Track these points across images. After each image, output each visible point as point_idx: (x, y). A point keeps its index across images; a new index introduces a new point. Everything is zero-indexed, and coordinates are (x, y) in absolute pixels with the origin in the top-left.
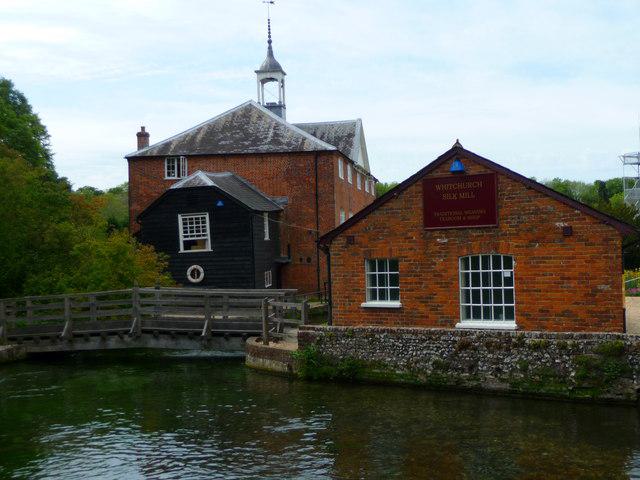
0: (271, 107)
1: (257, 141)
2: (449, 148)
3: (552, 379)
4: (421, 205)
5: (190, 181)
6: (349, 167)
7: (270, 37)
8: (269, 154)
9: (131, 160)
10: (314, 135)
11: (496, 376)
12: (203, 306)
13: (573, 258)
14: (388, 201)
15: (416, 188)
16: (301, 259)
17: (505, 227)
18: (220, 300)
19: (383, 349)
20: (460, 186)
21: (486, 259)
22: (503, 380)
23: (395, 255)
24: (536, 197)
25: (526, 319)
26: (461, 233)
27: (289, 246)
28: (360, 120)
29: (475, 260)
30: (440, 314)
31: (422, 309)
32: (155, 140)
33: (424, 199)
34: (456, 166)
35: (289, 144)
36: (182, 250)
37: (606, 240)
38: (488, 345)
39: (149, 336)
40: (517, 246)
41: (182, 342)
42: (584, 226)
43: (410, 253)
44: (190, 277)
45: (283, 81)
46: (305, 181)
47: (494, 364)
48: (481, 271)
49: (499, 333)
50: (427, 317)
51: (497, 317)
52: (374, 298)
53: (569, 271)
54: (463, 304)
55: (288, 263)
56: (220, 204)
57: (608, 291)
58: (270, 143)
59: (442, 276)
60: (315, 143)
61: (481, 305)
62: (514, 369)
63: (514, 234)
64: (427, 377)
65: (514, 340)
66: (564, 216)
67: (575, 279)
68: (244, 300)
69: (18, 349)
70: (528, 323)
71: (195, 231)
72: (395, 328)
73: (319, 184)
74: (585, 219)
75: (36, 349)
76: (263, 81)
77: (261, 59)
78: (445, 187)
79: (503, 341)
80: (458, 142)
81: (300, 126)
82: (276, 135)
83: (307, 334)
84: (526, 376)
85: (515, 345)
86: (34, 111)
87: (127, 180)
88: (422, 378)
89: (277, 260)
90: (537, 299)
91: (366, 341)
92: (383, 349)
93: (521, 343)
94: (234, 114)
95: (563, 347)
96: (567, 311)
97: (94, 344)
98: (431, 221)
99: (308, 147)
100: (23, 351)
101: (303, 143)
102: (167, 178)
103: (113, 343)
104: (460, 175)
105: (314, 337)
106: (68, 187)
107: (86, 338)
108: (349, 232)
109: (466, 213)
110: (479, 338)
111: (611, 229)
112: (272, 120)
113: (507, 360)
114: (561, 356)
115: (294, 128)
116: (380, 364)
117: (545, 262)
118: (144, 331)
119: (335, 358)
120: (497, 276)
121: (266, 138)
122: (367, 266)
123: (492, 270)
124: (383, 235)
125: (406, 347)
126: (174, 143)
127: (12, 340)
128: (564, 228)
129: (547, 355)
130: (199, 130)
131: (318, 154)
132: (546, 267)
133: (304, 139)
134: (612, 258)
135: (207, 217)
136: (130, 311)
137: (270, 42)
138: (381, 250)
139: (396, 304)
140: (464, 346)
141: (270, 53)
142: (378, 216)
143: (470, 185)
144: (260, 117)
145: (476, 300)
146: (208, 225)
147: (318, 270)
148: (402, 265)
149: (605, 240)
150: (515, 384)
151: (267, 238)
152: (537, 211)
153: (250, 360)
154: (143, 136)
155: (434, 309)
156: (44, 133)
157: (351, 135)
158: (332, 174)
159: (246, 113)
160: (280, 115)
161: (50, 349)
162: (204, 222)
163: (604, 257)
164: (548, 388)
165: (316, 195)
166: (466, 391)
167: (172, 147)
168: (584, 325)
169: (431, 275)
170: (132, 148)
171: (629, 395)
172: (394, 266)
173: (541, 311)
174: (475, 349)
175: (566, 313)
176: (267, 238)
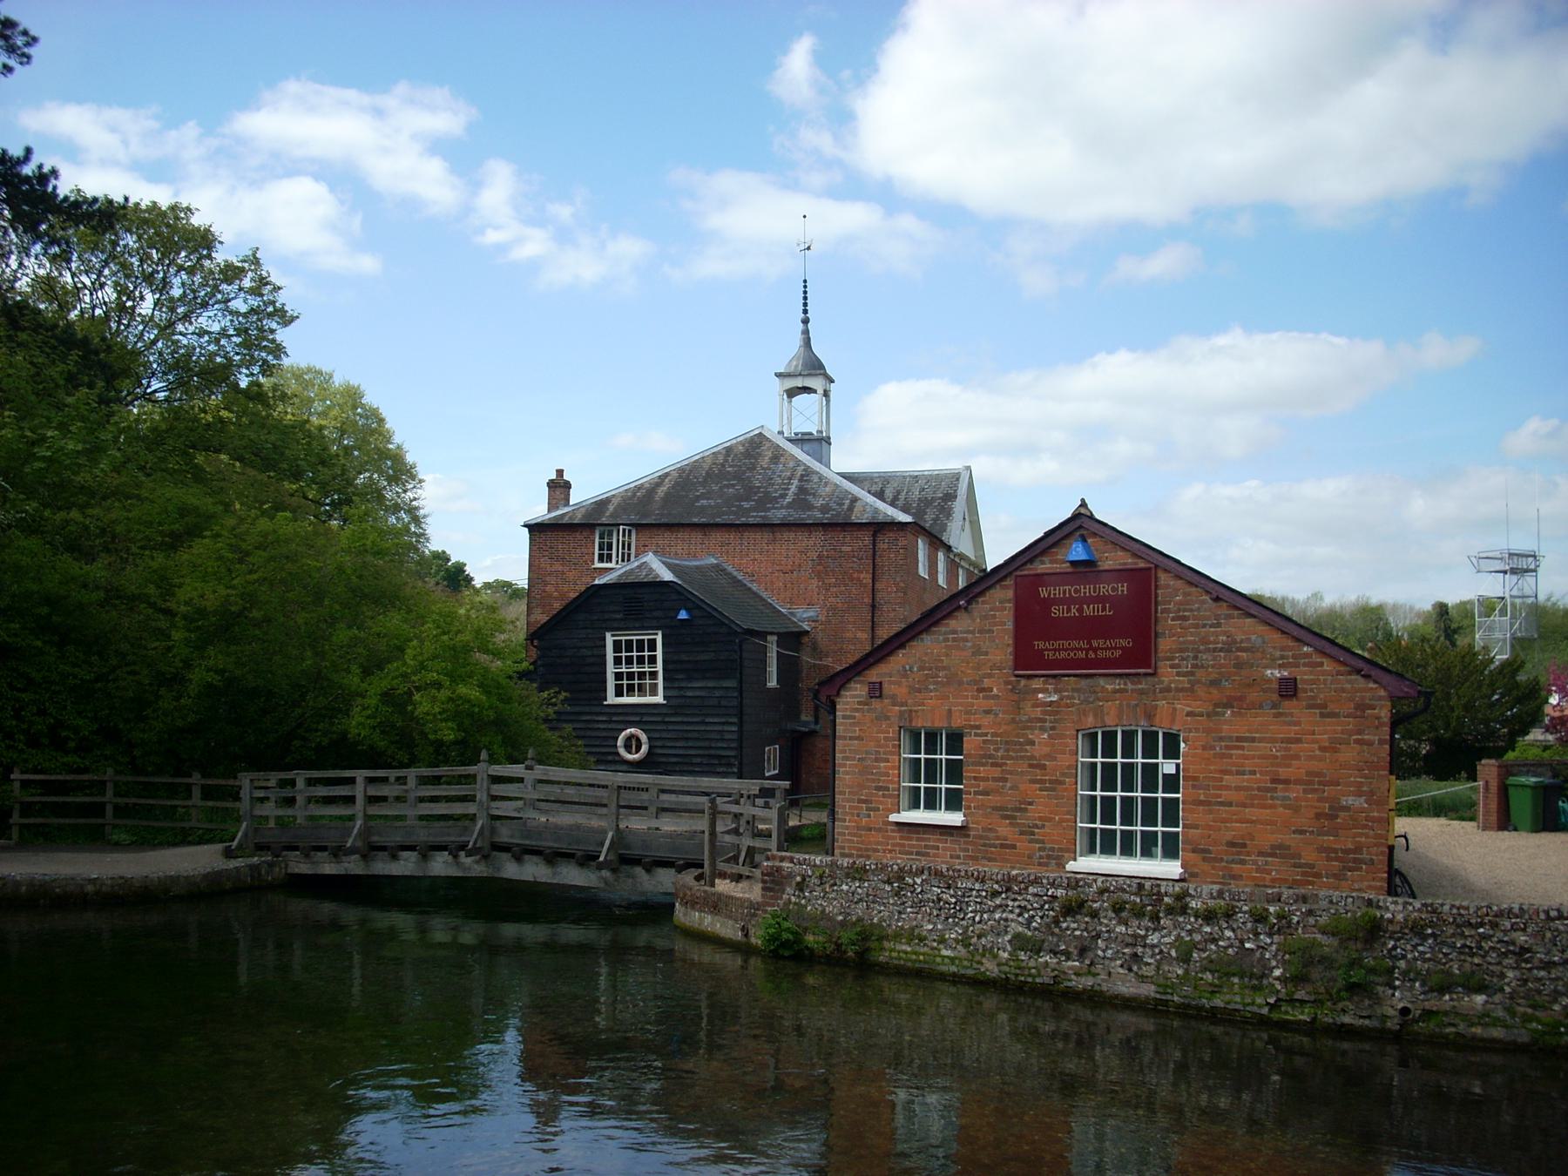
0: (802, 440)
1: (766, 501)
3: (1236, 980)
4: (1010, 626)
5: (631, 571)
6: (941, 556)
7: (805, 312)
8: (786, 526)
9: (535, 529)
10: (880, 495)
11: (1130, 970)
13: (1298, 741)
14: (948, 616)
15: (544, 562)
17: (1167, 674)
18: (645, 796)
19: (918, 905)
20: (1086, 590)
21: (1129, 737)
22: (1142, 979)
23: (957, 722)
24: (1229, 617)
25: (1201, 857)
26: (1084, 683)
29: (1109, 737)
30: (1037, 841)
31: (1004, 829)
32: (580, 495)
33: (1016, 610)
34: (1077, 552)
35: (825, 509)
36: (612, 699)
37: (1362, 707)
38: (1118, 908)
39: (505, 856)
40: (1188, 714)
41: (565, 871)
42: (1321, 676)
43: (986, 720)
44: (622, 751)
45: (826, 394)
47: (1127, 945)
48: (1119, 760)
49: (1140, 883)
50: (1014, 847)
51: (1147, 853)
52: (915, 805)
53: (1289, 766)
55: (813, 733)
56: (683, 615)
58: (789, 506)
59: (1043, 767)
61: (1118, 827)
62: (1164, 957)
63: (1182, 690)
65: (1166, 899)
66: (1282, 657)
67: (1297, 782)
68: (688, 798)
69: (271, 865)
70: (1206, 867)
73: (878, 586)
74: (1322, 664)
75: (304, 868)
76: (792, 393)
77: (787, 352)
79: (1145, 902)
80: (1083, 504)
81: (844, 476)
82: (801, 490)
83: (779, 869)
84: (1187, 971)
86: (397, 439)
88: (990, 968)
89: (790, 726)
90: (1224, 821)
91: (888, 888)
92: (918, 905)
94: (729, 450)
95: (1260, 918)
96: (1280, 847)
97: (406, 865)
98: (1026, 659)
101: (851, 508)
102: (598, 565)
103: (440, 866)
105: (791, 876)
107: (394, 853)
108: (874, 675)
109: (1095, 644)
110: (1102, 892)
111: (1372, 685)
112: (798, 462)
113: (1153, 938)
114: (1257, 934)
116: (914, 936)
117: (1242, 748)
119: (830, 919)
120: (1151, 771)
122: (905, 741)
123: (1140, 760)
124: (936, 683)
126: (615, 502)
127: (261, 848)
129: (1228, 933)
132: (1246, 757)
133: (855, 500)
134: (1370, 743)
136: (471, 808)
137: (806, 321)
138: (933, 713)
139: (955, 819)
141: (807, 342)
142: (928, 645)
146: (659, 653)
148: (970, 743)
150: (1164, 987)
152: (1230, 647)
153: (682, 915)
154: (559, 487)
155: (1027, 832)
156: (413, 477)
157: (950, 497)
159: (756, 444)
161: (329, 869)
162: (629, 643)
163: (1357, 742)
164: (1228, 997)
165: (873, 606)
166: (1073, 996)
167: (611, 508)
169: (1023, 767)
170: (539, 510)
171: (1385, 1017)
173: (1231, 844)
174: (1094, 914)
175: (1278, 851)
176: (773, 683)
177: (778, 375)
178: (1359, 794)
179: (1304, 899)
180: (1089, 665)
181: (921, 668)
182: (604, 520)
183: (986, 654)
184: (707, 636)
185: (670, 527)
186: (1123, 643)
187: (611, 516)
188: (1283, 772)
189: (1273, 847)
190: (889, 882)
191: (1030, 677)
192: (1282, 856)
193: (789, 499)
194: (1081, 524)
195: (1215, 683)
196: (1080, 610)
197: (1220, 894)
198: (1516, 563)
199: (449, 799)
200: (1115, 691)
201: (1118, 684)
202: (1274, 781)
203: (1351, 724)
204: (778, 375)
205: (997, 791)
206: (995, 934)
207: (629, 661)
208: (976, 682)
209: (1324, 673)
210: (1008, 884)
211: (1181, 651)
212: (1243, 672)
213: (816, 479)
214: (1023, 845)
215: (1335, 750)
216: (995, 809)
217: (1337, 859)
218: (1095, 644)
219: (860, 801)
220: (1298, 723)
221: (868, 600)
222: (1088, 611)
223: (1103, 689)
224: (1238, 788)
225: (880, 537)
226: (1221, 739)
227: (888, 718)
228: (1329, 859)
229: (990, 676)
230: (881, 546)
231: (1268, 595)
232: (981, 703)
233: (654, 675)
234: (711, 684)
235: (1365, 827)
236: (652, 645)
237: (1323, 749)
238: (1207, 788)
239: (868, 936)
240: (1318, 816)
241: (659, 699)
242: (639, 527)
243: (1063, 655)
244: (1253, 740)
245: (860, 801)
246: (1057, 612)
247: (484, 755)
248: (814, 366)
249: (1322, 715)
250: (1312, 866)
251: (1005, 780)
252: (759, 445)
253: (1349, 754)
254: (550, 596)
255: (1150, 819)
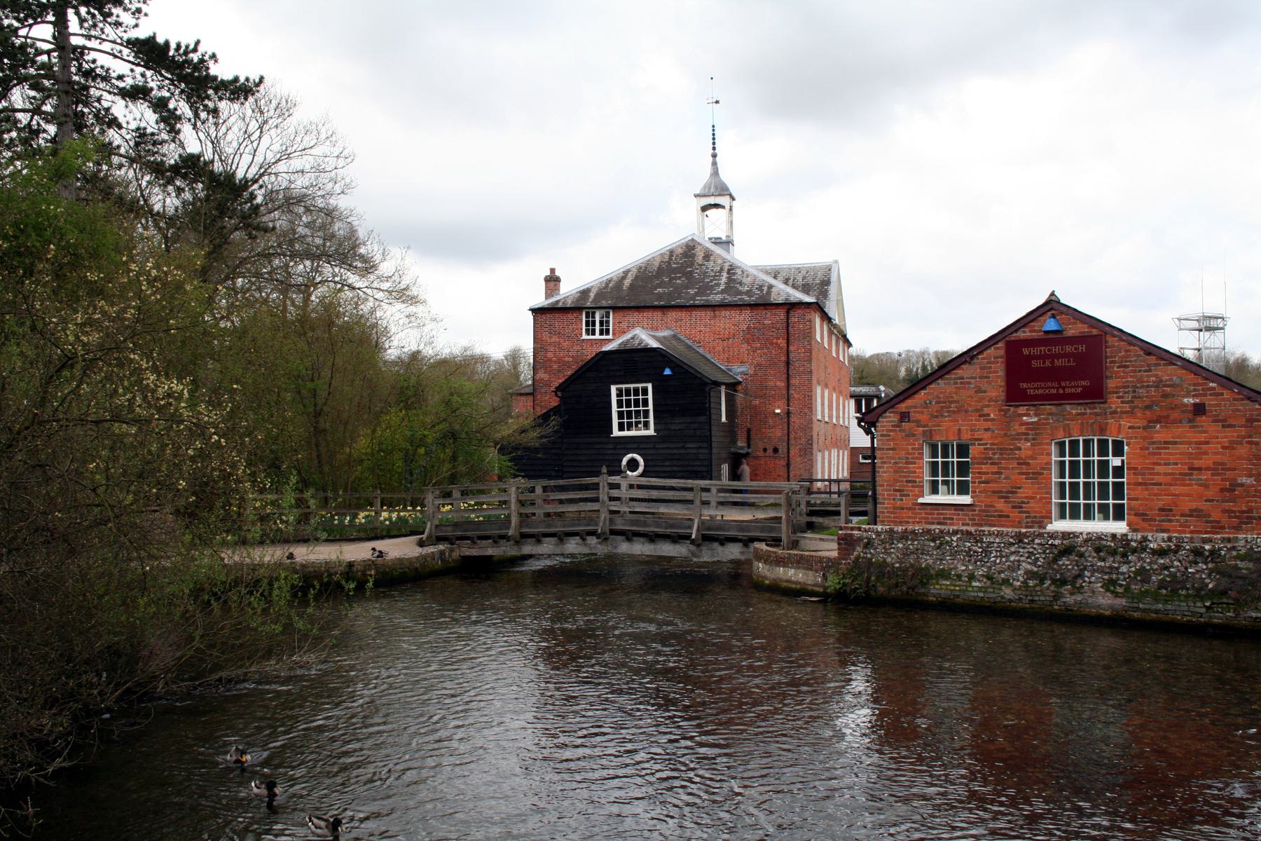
0: (717, 242)
1: (705, 289)
2: (1041, 300)
4: (1001, 373)
7: (714, 149)
9: (537, 312)
12: (749, 431)
13: (1207, 443)
15: (999, 350)
16: (765, 450)
17: (1114, 402)
19: (954, 554)
22: (1116, 595)
23: (966, 437)
24: (1156, 365)
25: (1141, 519)
27: (749, 431)
28: (836, 262)
31: (1000, 505)
32: (568, 289)
34: (1051, 325)
35: (749, 293)
36: (616, 433)
38: (1098, 550)
39: (619, 538)
45: (731, 209)
46: (772, 344)
54: (1055, 500)
55: (748, 454)
56: (667, 372)
57: (1253, 486)
58: (723, 292)
59: (1028, 464)
60: (783, 292)
61: (1067, 501)
64: (1015, 589)
67: (1207, 469)
71: (632, 417)
72: (972, 529)
73: (791, 348)
76: (704, 209)
78: (1035, 351)
80: (1053, 294)
81: (756, 267)
82: (730, 280)
85: (1134, 551)
87: (403, 337)
92: (954, 554)
93: (1142, 546)
94: (671, 252)
96: (1196, 510)
98: (1015, 395)
99: (776, 298)
100: (456, 555)
101: (769, 292)
104: (1055, 338)
105: (860, 539)
106: (378, 347)
108: (903, 407)
109: (1063, 384)
110: (1086, 541)
113: (1124, 569)
115: (754, 272)
118: (613, 532)
120: (1104, 465)
121: (718, 285)
122: (926, 450)
125: (986, 552)
127: (440, 539)
128: (1195, 405)
129: (1176, 563)
130: (626, 273)
131: (791, 306)
133: (771, 287)
135: (650, 386)
137: (714, 156)
138: (948, 430)
139: (966, 499)
140: (1067, 551)
141: (715, 173)
143: (1068, 349)
144: (708, 256)
145: (1074, 495)
146: (650, 396)
147: (788, 465)
148: (973, 451)
149: (1248, 421)
151: (724, 419)
152: (1159, 384)
154: (552, 281)
155: (1017, 507)
157: (826, 282)
158: (809, 334)
159: (690, 248)
160: (728, 251)
162: (628, 392)
165: (788, 363)
167: (592, 295)
168: (1217, 527)
170: (540, 300)
172: (963, 450)
173: (1162, 510)
174: (1081, 555)
175: (1195, 513)
176: (724, 419)
177: (696, 196)
178: (1250, 476)
179: (1229, 540)
180: (1059, 398)
181: (937, 402)
182: (588, 304)
183: (985, 392)
184: (683, 388)
185: (638, 308)
186: (1084, 383)
187: (594, 301)
188: (1197, 463)
189: (1191, 510)
190: (934, 540)
191: (1017, 406)
192: (1198, 516)
193: (722, 287)
194: (1052, 306)
195: (1148, 407)
196: (1052, 362)
197: (1170, 539)
198: (1206, 323)
199: (672, 488)
200: (1078, 414)
201: (1080, 410)
202: (1190, 469)
203: (1243, 431)
204: (696, 196)
205: (995, 481)
206: (1014, 572)
207: (628, 404)
208: (977, 410)
209: (1223, 400)
210: (1019, 538)
211: (1124, 387)
212: (1169, 400)
213: (739, 272)
214: (1014, 514)
215: (1233, 448)
216: (994, 492)
217: (1236, 517)
218: (1063, 384)
219: (895, 490)
220: (1205, 432)
221: (783, 358)
222: (1058, 363)
223: (1070, 413)
224: (1165, 474)
225: (792, 313)
226: (1153, 443)
227: (914, 435)
228: (1230, 517)
229: (988, 406)
230: (793, 320)
231: (457, 351)
232: (982, 424)
233: (646, 413)
234: (689, 420)
235: (1254, 496)
236: (645, 391)
237: (1223, 448)
238: (1144, 474)
239: (925, 576)
240: (1222, 490)
241: (651, 432)
242: (615, 309)
243: (1041, 392)
244: (1176, 443)
245: (895, 490)
246: (1035, 364)
247: (604, 470)
248: (723, 190)
249: (1223, 426)
250: (1218, 522)
251: (1000, 473)
252: (693, 248)
253: (1243, 451)
254: (550, 360)
255: (1103, 494)
